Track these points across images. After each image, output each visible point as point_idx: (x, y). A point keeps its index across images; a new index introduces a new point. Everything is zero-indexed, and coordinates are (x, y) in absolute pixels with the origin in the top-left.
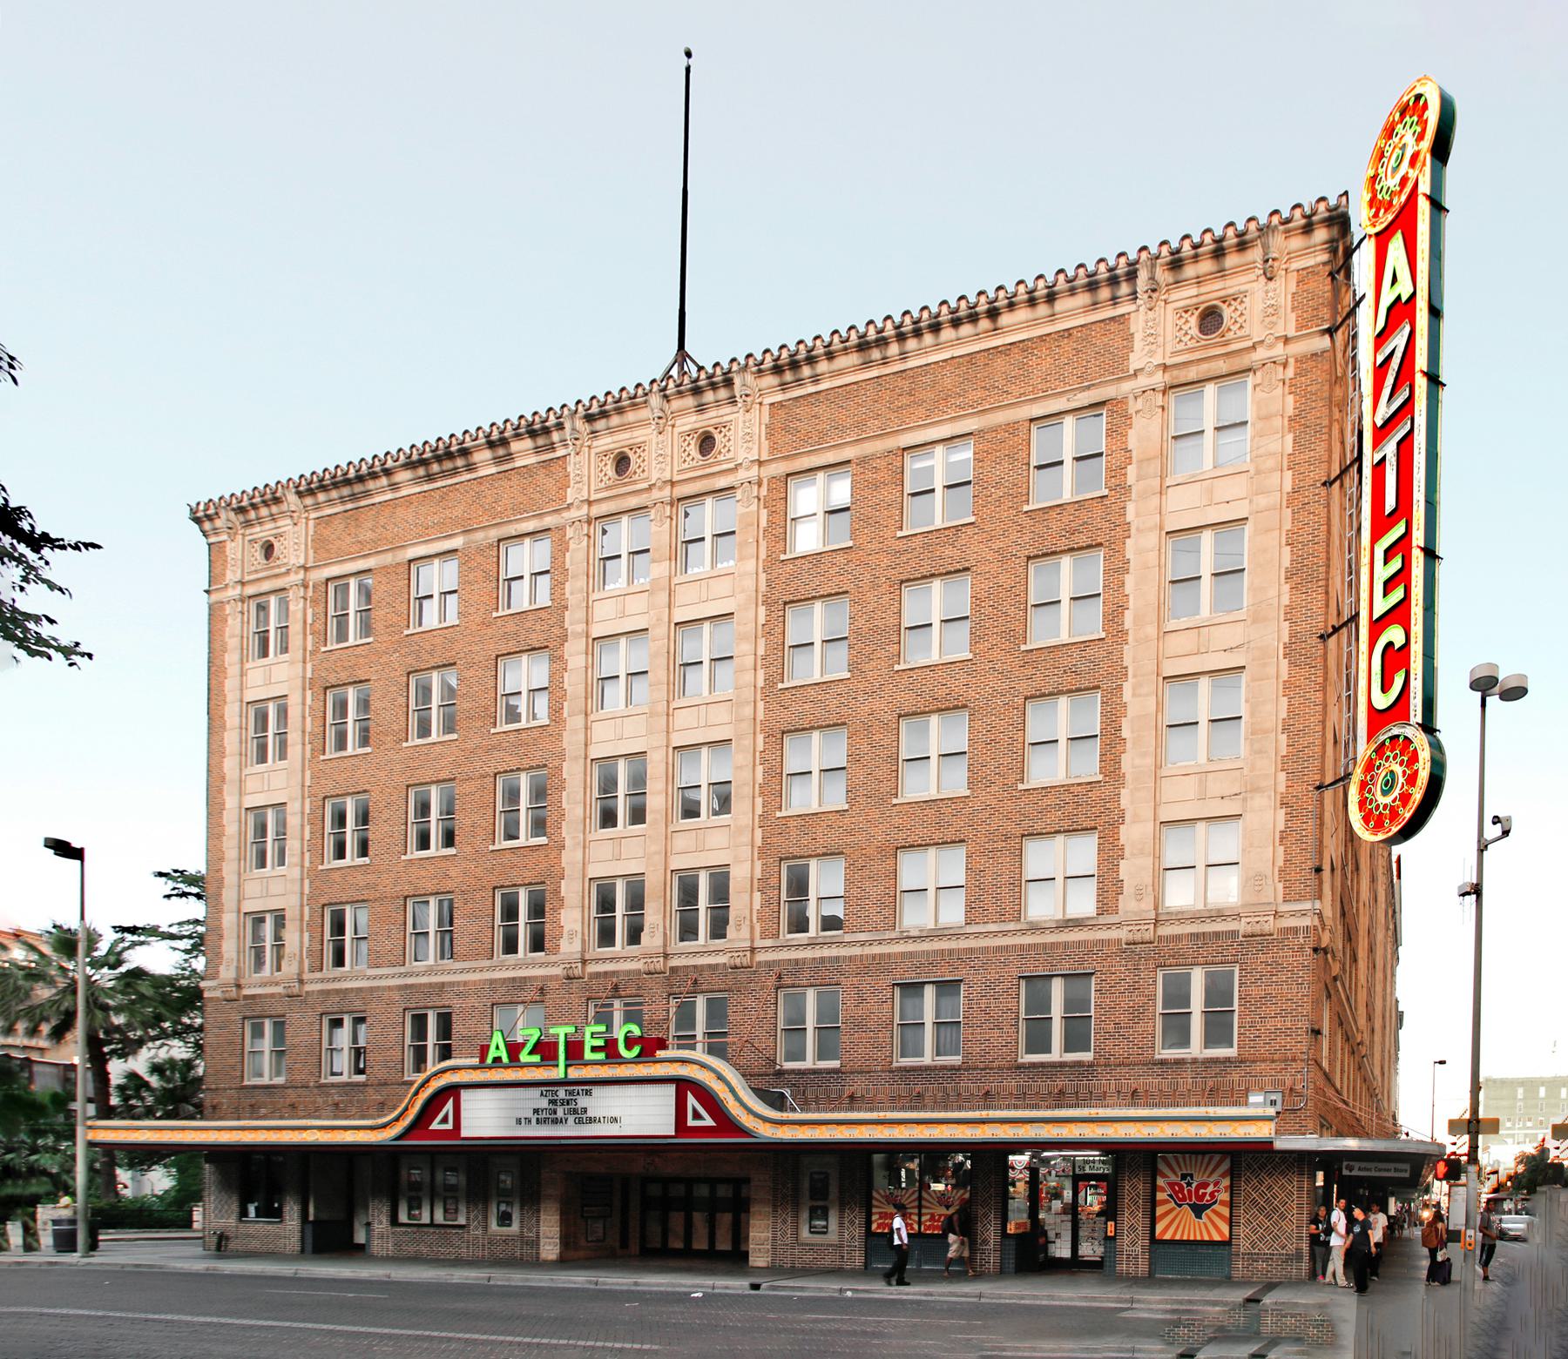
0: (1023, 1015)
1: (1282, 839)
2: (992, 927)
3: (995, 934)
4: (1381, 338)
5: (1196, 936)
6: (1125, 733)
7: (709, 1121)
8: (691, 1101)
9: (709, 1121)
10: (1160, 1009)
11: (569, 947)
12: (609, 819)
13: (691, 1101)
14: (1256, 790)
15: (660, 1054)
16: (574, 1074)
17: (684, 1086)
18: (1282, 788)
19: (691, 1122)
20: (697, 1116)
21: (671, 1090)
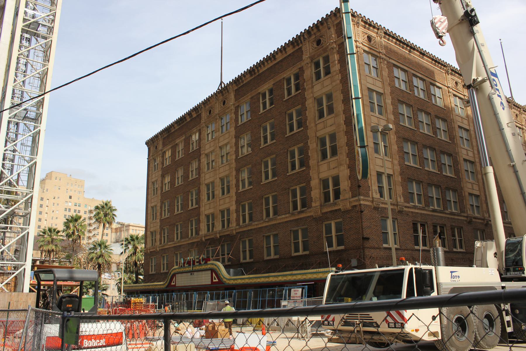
0: (292, 241)
1: (349, 178)
2: (283, 216)
3: (284, 218)
4: (14, 238)
5: (331, 211)
6: (310, 155)
7: (217, 280)
8: (214, 275)
9: (217, 280)
10: (324, 235)
11: (315, 204)
12: (324, 156)
13: (214, 275)
14: (341, 165)
15: (209, 262)
16: (194, 268)
17: (213, 271)
18: (348, 163)
19: (214, 281)
20: (215, 279)
21: (210, 272)
